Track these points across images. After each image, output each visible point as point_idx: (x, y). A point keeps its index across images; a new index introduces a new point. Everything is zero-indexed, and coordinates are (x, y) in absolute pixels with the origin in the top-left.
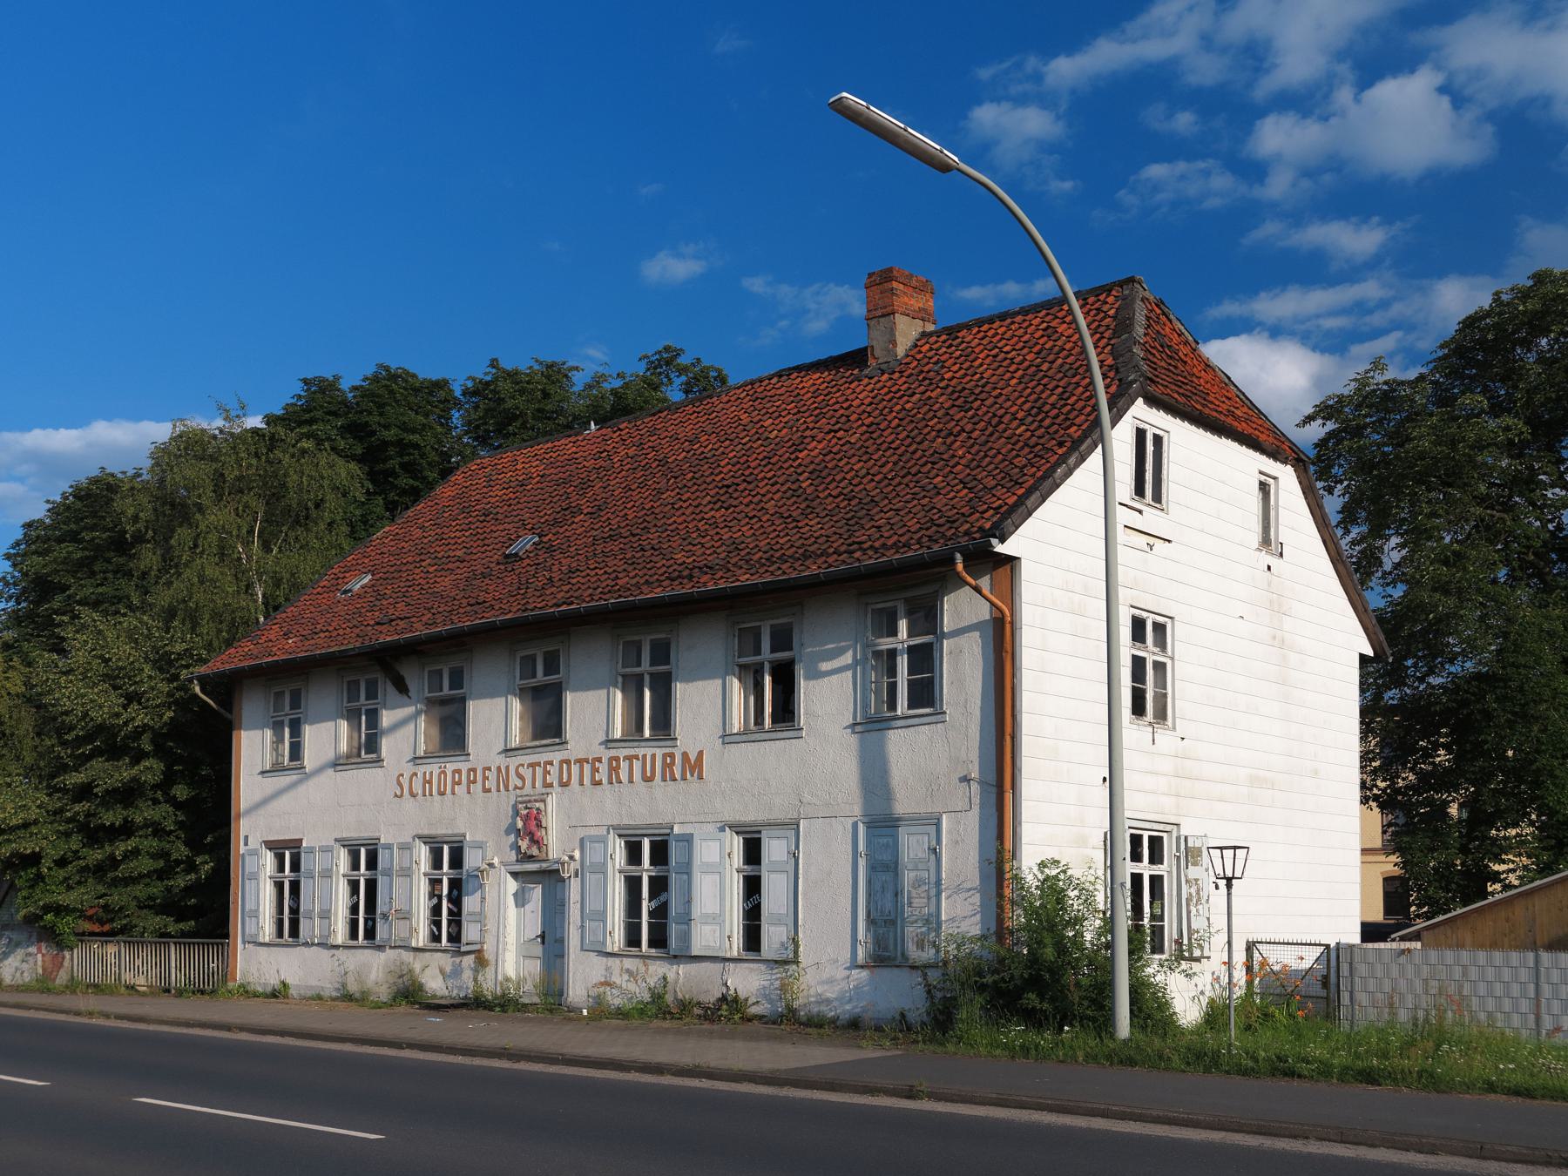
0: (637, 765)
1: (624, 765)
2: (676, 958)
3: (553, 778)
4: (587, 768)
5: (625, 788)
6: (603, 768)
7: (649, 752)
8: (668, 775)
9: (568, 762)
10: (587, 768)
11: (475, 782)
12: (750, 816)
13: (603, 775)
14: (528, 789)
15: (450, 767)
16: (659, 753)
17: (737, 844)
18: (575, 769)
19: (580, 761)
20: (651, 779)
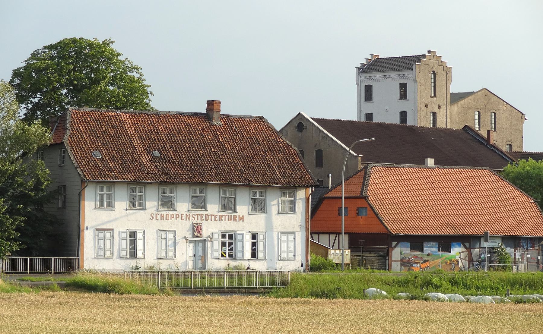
0: (227, 217)
1: (224, 217)
2: (236, 259)
3: (204, 218)
4: (213, 217)
5: (223, 222)
6: (218, 217)
7: (230, 215)
8: (235, 219)
9: (208, 215)
10: (213, 217)
11: (173, 217)
12: (255, 230)
13: (218, 218)
14: (196, 220)
15: (170, 213)
16: (232, 215)
17: (508, 146)
18: (210, 217)
19: (211, 215)
20: (231, 220)
